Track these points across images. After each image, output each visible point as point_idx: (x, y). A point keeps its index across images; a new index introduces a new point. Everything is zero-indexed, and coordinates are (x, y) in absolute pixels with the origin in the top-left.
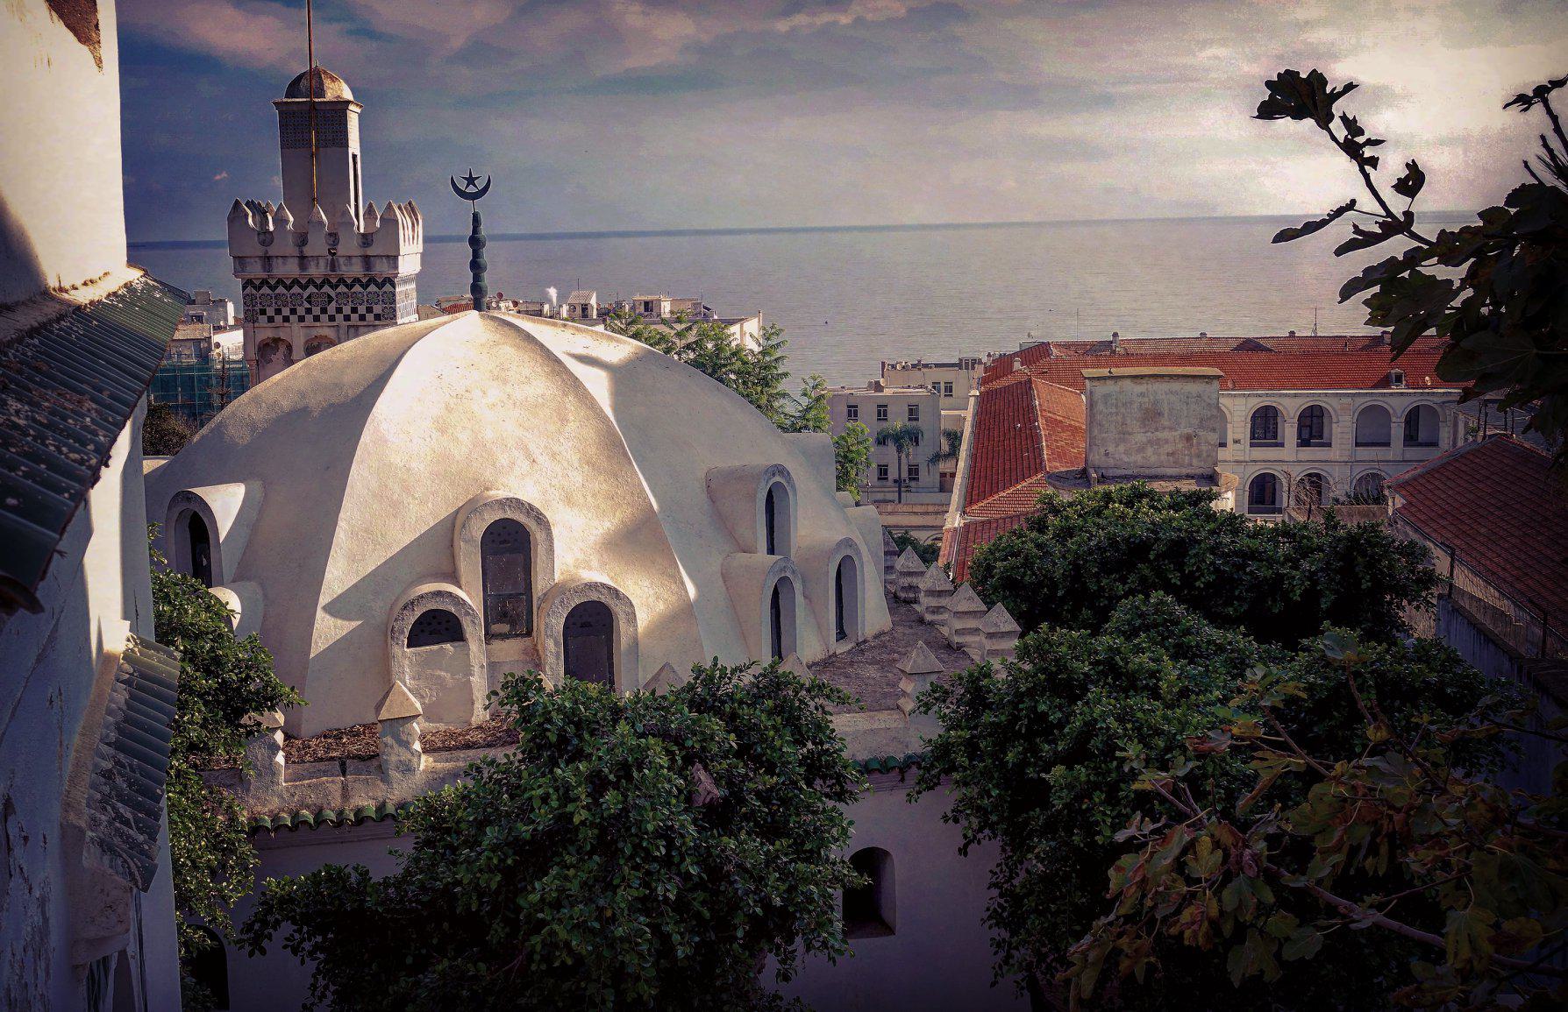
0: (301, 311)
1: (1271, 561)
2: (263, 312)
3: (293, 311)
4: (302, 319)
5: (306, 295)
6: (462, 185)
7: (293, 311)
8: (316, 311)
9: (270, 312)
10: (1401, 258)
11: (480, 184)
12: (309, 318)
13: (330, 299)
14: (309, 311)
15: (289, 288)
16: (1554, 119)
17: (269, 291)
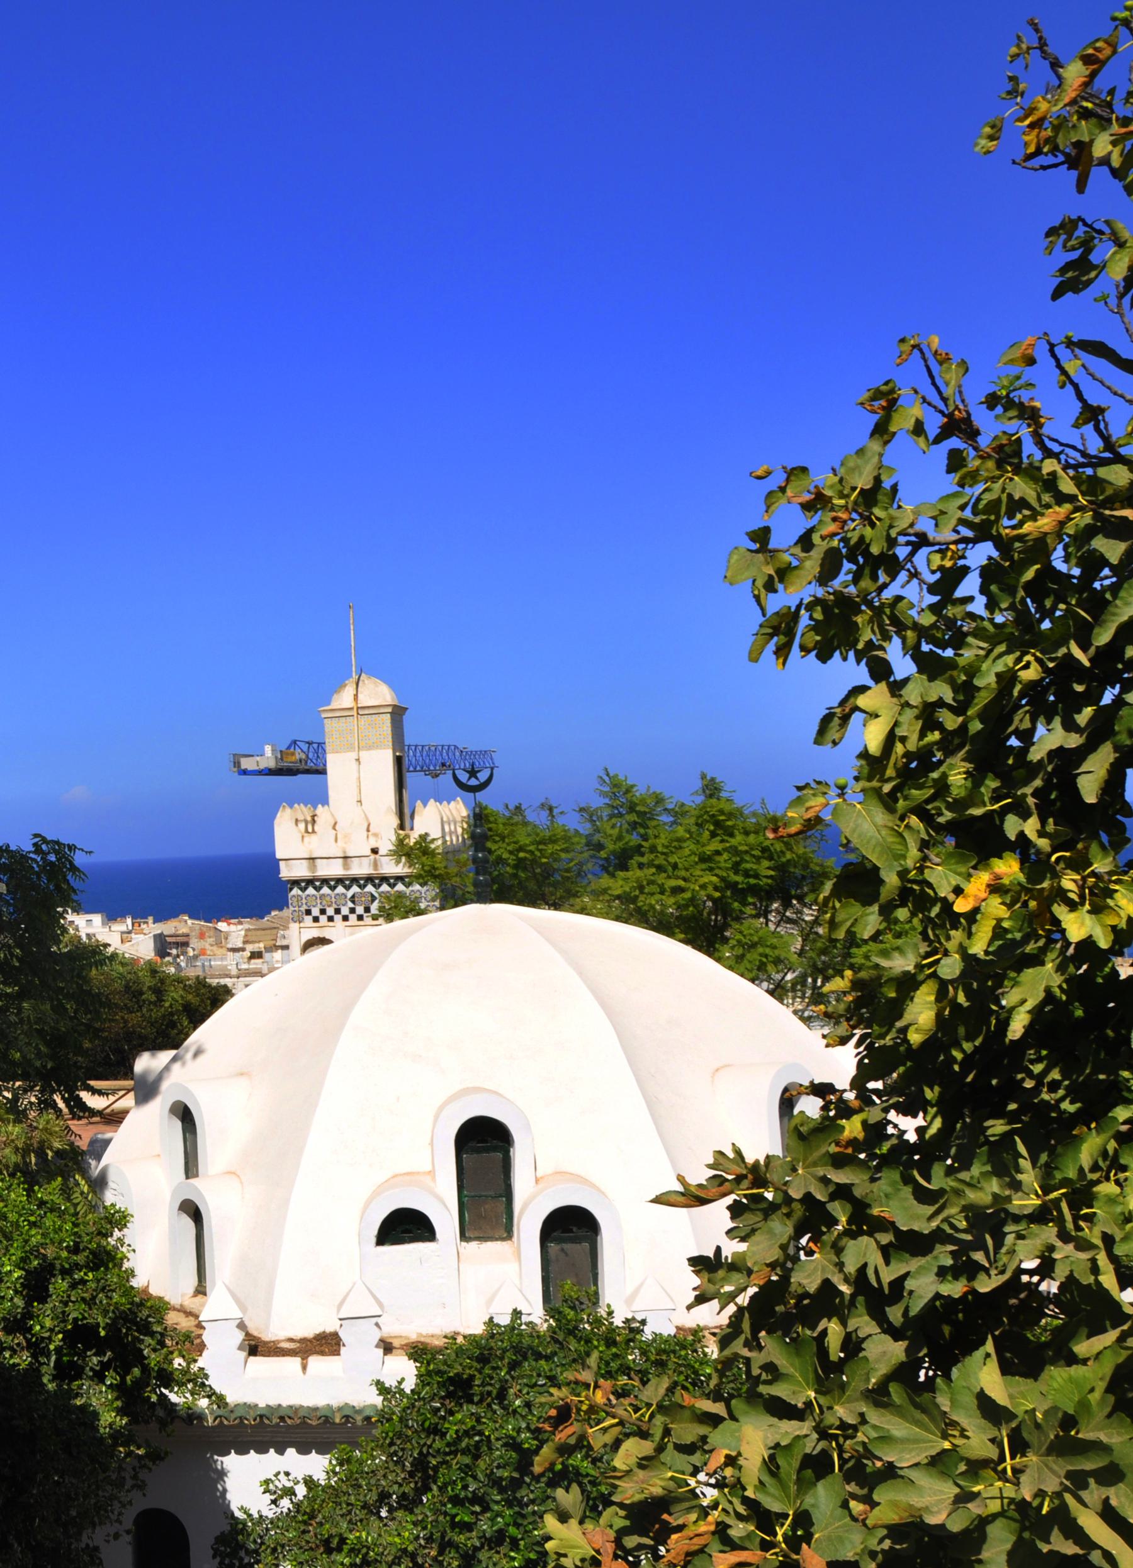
0: (345, 911)
1: (1011, 957)
2: (308, 912)
3: (338, 911)
4: (345, 918)
5: (350, 894)
6: (463, 777)
7: (338, 911)
8: (360, 910)
9: (316, 912)
10: (272, 1451)
11: (483, 776)
12: (353, 917)
13: (373, 898)
14: (352, 911)
15: (333, 888)
16: (1059, 366)
17: (300, 892)
